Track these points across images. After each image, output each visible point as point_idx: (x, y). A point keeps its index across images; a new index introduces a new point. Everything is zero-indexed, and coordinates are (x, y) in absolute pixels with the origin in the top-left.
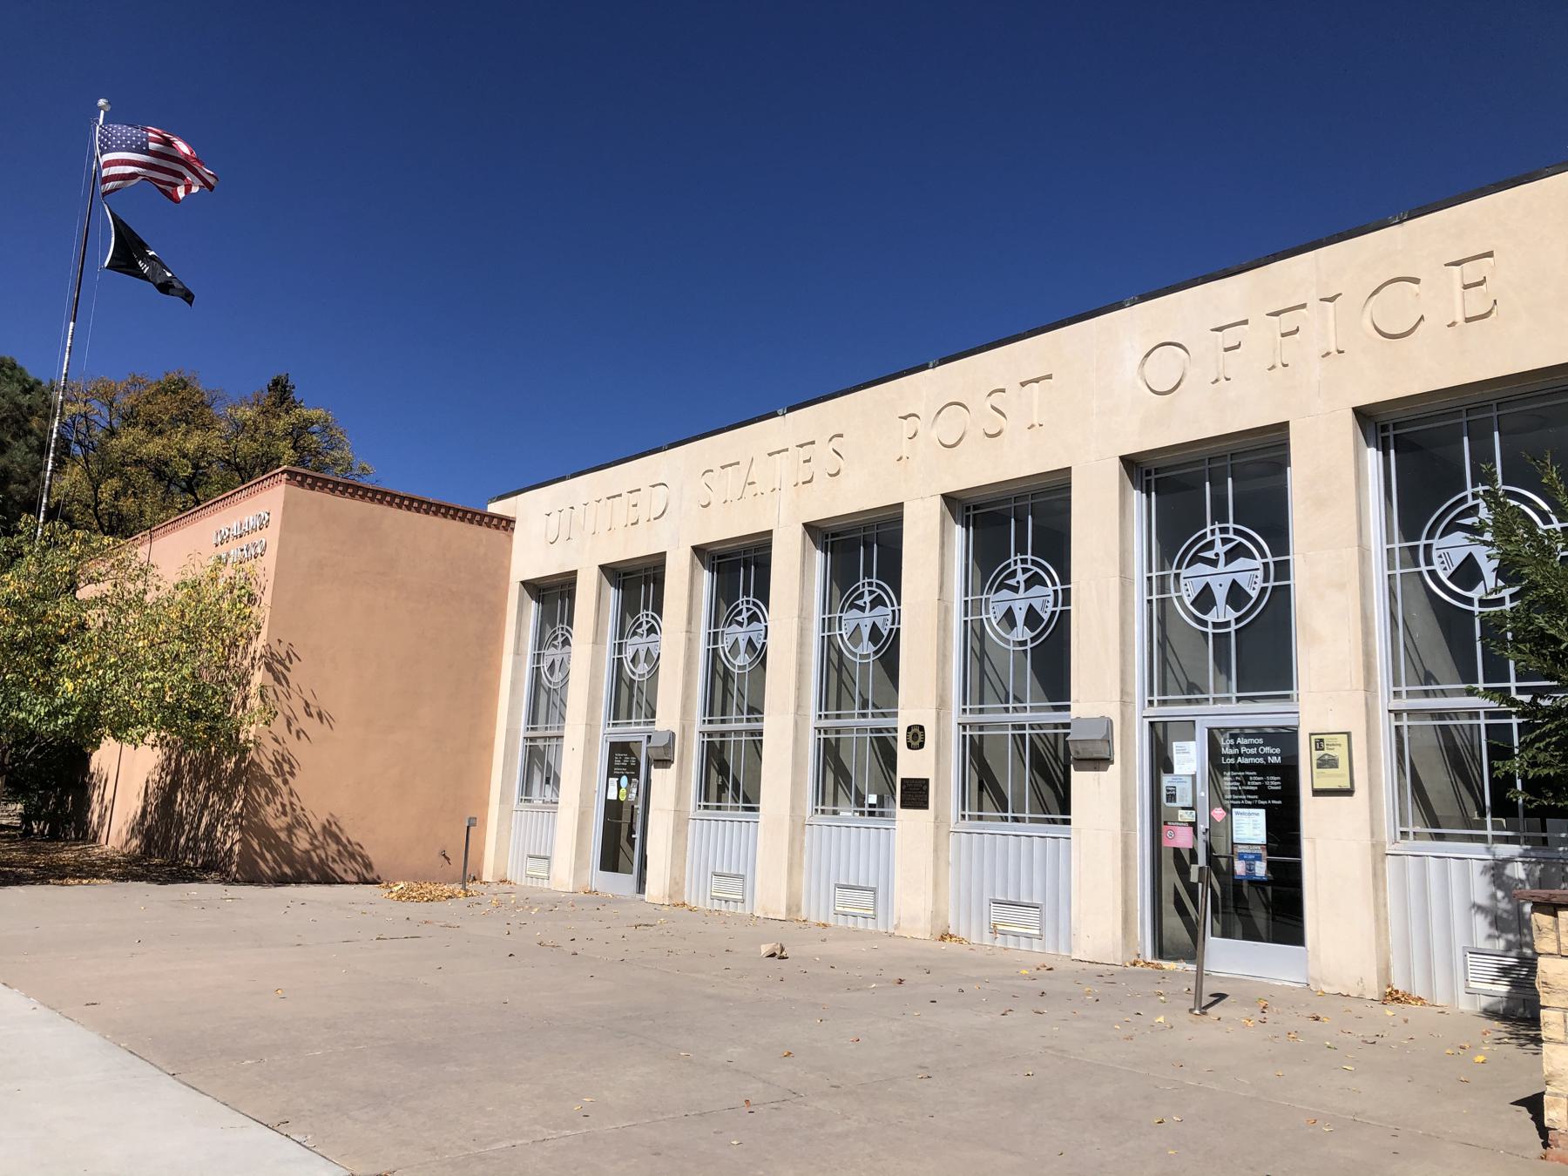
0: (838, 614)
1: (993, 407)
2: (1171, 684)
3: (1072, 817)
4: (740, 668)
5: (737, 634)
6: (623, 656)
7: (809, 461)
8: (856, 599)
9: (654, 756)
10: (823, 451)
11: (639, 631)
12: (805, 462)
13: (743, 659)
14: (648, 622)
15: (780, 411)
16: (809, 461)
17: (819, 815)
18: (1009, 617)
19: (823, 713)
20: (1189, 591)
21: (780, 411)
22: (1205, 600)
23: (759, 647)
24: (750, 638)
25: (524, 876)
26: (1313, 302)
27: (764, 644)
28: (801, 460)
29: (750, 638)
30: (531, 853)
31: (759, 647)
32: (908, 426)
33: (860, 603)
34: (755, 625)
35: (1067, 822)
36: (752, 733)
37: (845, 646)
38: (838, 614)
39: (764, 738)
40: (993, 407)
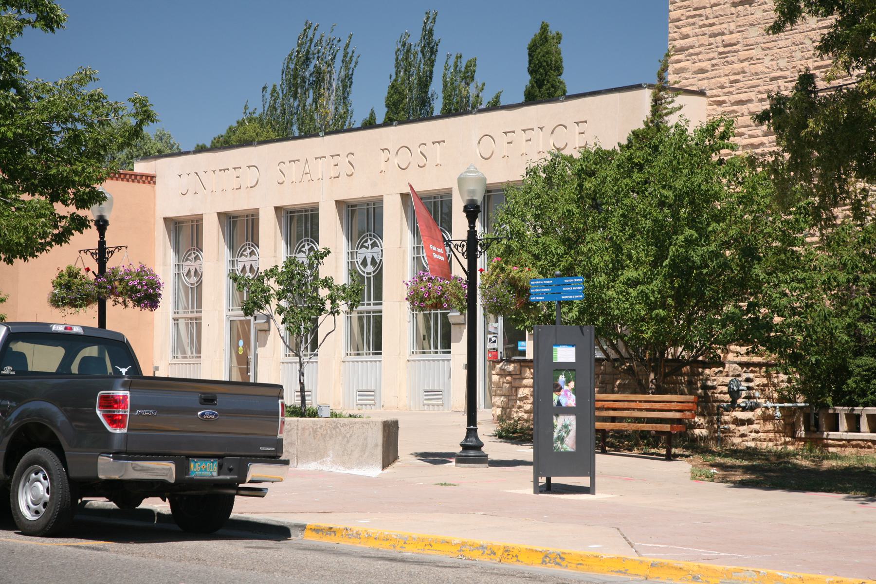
0: (356, 250)
1: (421, 152)
2: (234, 304)
3: (202, 355)
4: (368, 274)
5: (190, 265)
6: (421, 255)
7: (337, 165)
8: (364, 242)
9: (259, 328)
10: (343, 160)
11: (190, 258)
12: (527, 141)
13: (370, 268)
14: (249, 249)
15: (321, 134)
16: (337, 165)
17: (288, 357)
18: (365, 260)
19: (231, 308)
20: (360, 259)
21: (321, 134)
22: (364, 263)
23: (378, 262)
24: (373, 257)
25: (422, 405)
26: (536, 128)
27: (381, 260)
28: (333, 164)
29: (373, 257)
30: (360, 389)
31: (378, 262)
32: (384, 156)
33: (366, 244)
34: (253, 257)
35: (450, 352)
36: (196, 319)
37: (359, 268)
38: (356, 250)
39: (383, 314)
40: (421, 152)
